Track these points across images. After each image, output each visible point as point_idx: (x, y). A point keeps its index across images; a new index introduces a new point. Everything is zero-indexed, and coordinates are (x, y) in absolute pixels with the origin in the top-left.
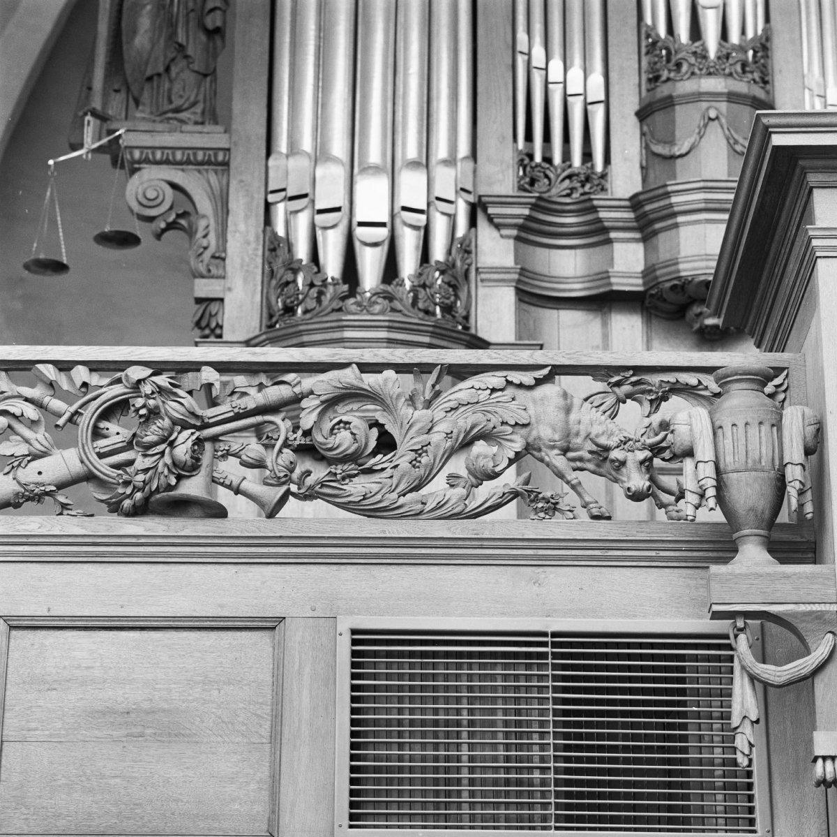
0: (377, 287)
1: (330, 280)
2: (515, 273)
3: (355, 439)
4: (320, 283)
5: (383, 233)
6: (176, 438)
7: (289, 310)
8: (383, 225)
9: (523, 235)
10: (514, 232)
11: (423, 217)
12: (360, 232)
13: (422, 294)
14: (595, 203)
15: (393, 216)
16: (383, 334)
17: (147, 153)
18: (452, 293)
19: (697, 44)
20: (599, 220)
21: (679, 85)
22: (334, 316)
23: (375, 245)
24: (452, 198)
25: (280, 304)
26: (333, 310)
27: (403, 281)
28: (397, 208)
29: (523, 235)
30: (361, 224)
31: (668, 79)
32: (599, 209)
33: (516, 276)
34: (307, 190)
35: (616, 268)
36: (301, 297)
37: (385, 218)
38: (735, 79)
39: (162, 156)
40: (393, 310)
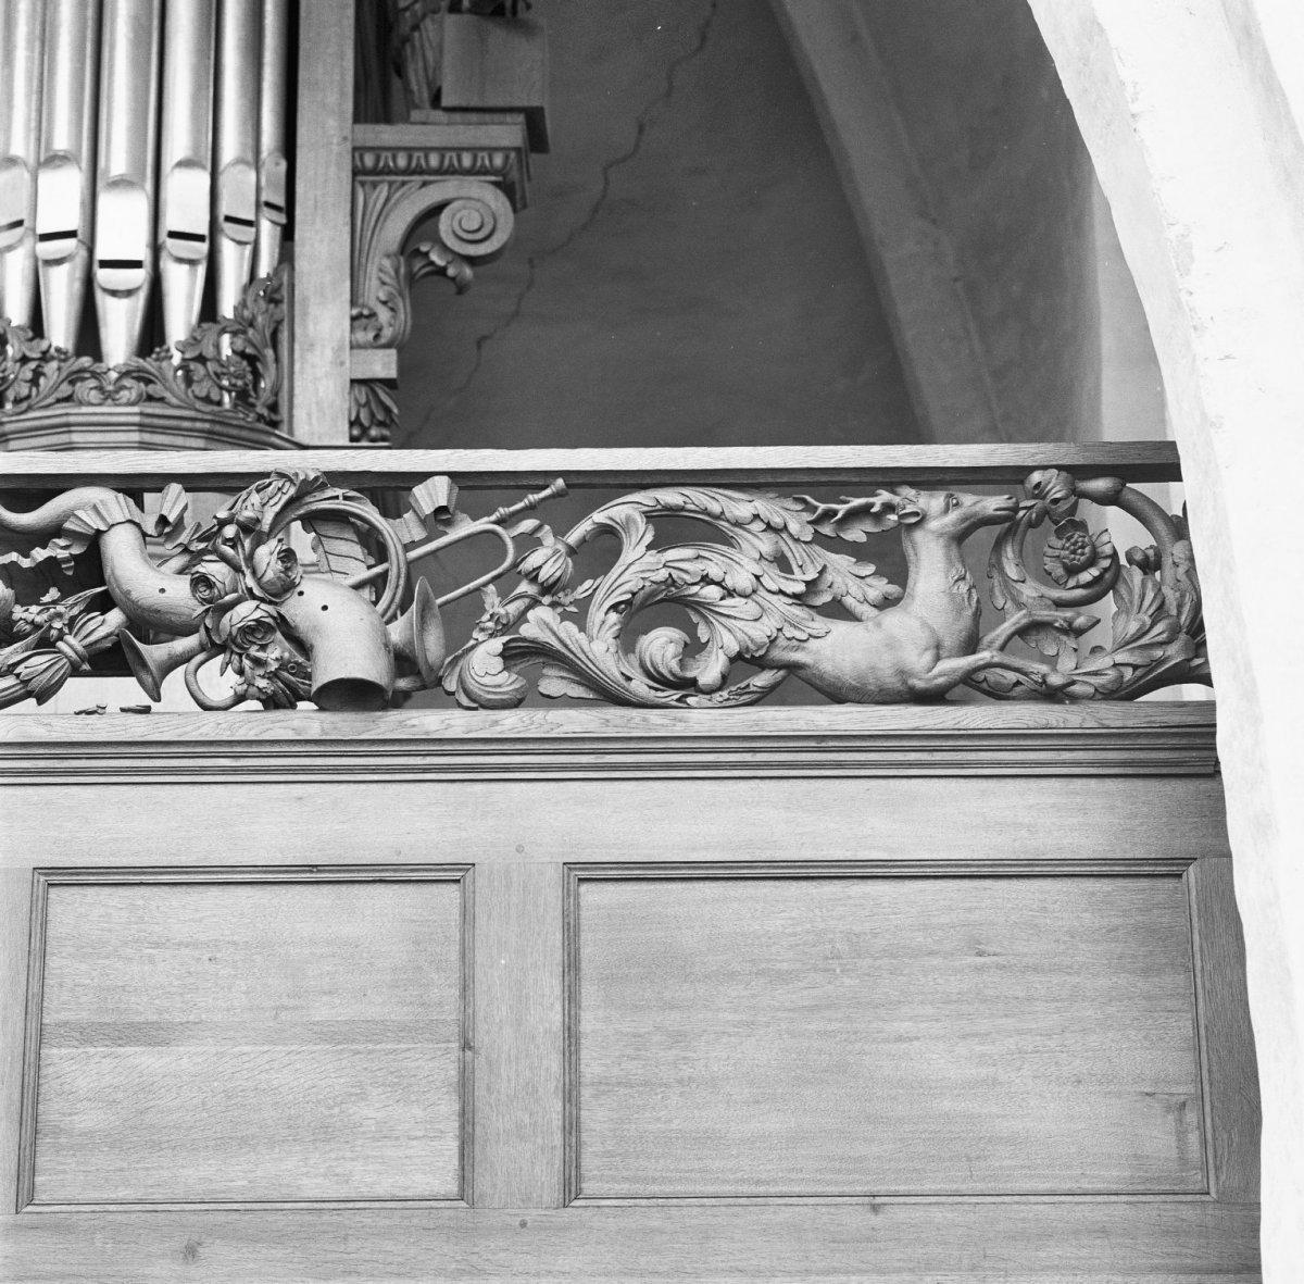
4: (39, 355)
5: (139, 277)
8: (137, 264)
12: (103, 276)
13: (198, 370)
15: (156, 249)
16: (135, 437)
17: (451, 158)
18: (248, 369)
22: (59, 410)
23: (129, 293)
26: (59, 401)
30: (105, 264)
34: (23, 215)
39: (442, 162)
40: (150, 398)
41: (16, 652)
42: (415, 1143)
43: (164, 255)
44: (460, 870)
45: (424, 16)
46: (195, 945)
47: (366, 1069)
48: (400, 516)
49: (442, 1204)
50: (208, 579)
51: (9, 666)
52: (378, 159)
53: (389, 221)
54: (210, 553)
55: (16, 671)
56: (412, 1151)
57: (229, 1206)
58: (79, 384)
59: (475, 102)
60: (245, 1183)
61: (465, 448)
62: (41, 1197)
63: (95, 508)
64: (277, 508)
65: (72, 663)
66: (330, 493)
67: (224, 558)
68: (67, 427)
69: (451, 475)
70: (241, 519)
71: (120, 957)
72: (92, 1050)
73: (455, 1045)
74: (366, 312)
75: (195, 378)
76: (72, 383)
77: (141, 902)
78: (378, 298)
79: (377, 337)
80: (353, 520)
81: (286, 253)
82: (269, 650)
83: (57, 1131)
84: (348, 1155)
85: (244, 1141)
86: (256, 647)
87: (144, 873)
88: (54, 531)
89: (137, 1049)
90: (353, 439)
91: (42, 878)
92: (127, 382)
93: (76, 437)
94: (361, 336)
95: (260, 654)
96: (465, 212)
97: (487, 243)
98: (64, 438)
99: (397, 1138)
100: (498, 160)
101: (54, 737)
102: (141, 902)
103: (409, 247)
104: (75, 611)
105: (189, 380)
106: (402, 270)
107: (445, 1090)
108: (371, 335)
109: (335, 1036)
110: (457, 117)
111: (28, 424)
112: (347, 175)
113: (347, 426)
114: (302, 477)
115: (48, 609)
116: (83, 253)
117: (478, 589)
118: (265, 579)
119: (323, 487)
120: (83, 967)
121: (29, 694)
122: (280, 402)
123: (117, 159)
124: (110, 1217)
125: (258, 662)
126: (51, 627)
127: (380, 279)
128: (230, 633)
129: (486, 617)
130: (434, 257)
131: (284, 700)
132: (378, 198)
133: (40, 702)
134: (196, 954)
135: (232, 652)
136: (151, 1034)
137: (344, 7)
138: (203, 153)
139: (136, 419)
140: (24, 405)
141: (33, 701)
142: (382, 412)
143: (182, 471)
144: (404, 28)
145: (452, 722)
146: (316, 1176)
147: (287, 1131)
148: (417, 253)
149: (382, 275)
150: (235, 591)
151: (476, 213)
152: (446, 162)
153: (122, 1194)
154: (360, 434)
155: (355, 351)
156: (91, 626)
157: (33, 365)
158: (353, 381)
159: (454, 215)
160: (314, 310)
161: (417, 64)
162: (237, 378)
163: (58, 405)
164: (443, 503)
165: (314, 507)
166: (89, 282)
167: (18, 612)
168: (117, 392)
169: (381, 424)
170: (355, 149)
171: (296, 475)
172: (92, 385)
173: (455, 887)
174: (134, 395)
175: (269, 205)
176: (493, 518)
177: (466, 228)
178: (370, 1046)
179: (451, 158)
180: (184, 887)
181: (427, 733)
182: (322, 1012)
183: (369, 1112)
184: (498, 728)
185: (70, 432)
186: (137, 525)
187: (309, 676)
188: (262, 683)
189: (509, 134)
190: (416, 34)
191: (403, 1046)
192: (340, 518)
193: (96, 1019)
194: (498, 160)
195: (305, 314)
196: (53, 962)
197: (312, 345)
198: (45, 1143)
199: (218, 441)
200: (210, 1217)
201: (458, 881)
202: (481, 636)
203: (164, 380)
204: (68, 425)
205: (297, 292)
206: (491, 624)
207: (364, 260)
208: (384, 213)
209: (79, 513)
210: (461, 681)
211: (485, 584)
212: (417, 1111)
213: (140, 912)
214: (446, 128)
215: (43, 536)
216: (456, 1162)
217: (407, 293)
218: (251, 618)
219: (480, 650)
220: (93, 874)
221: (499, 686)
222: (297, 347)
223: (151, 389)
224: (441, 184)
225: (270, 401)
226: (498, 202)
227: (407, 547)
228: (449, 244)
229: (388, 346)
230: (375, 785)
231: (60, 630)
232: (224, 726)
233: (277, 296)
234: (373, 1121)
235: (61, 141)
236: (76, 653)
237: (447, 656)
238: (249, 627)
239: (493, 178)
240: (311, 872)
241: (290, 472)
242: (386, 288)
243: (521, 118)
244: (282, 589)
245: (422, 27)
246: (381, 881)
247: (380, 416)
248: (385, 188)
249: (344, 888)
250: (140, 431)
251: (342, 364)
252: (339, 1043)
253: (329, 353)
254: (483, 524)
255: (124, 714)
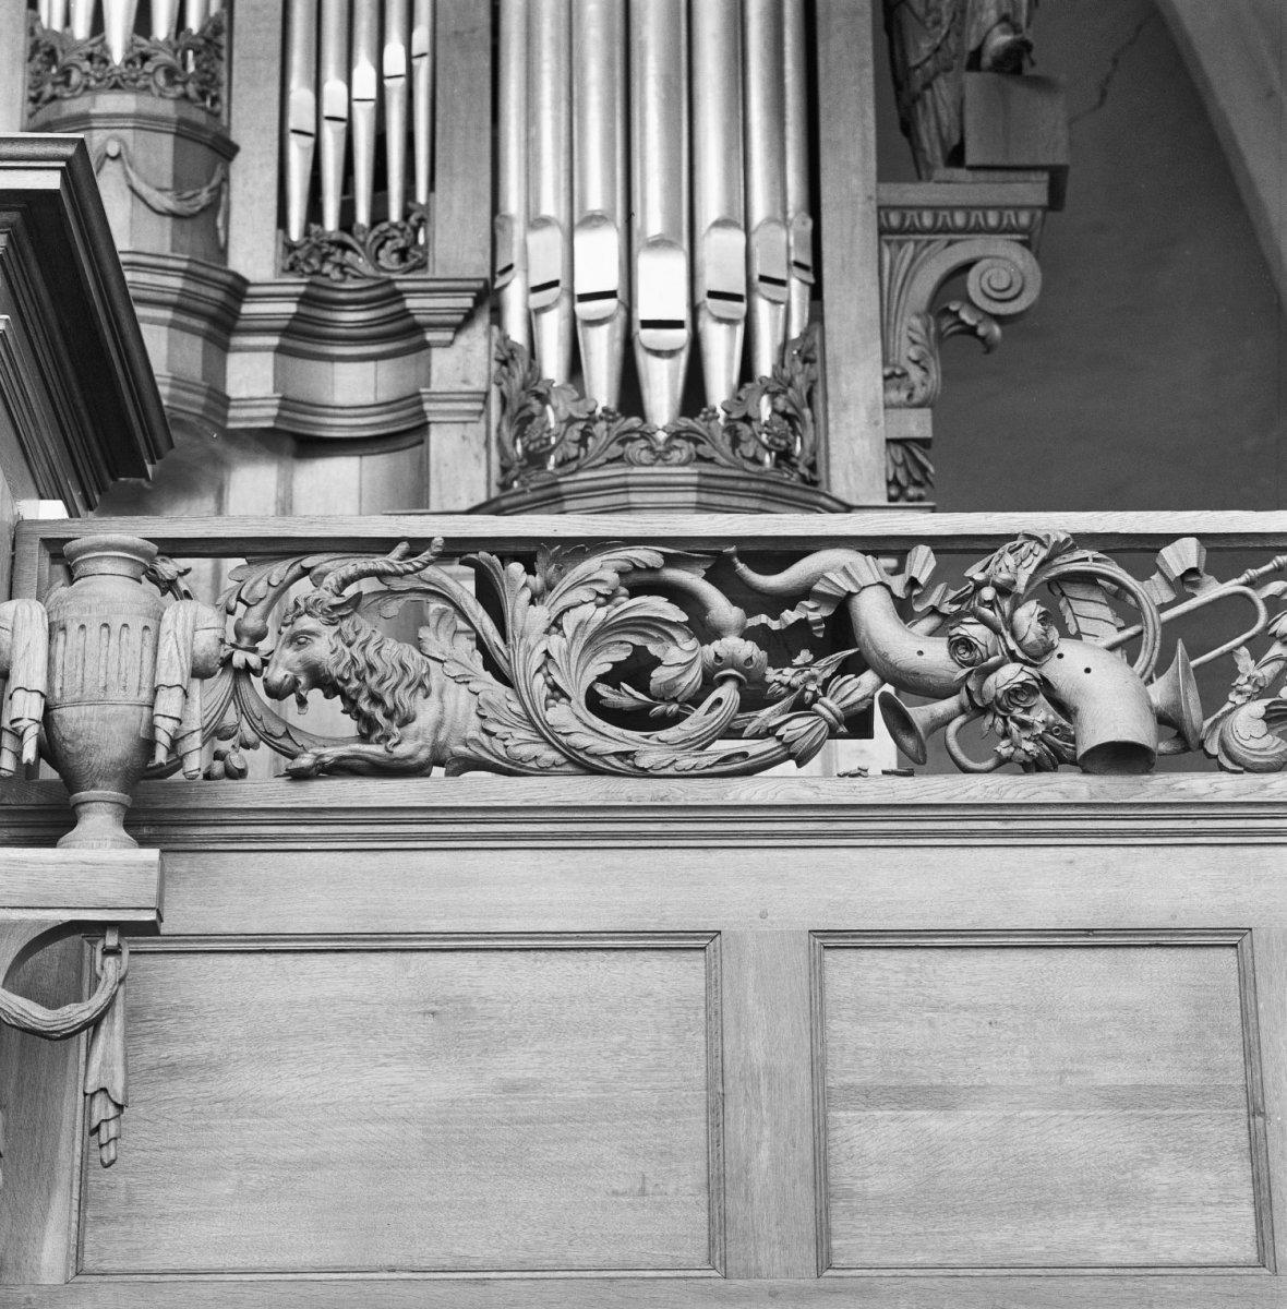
0: (674, 423)
1: (599, 411)
2: (272, 406)
3: (155, 691)
4: (585, 416)
5: (681, 337)
6: (950, 326)
7: (535, 459)
8: (678, 324)
9: (290, 343)
10: (274, 341)
11: (743, 306)
12: (646, 336)
14: (398, 286)
15: (694, 309)
16: (693, 497)
17: (977, 217)
18: (790, 429)
19: (95, 40)
20: (406, 313)
21: (66, 104)
23: (671, 354)
24: (781, 275)
25: (519, 448)
26: (610, 461)
27: (714, 411)
28: (701, 296)
29: (290, 343)
30: (647, 324)
31: (54, 98)
32: (405, 295)
33: (274, 412)
35: (434, 387)
36: (553, 441)
37: (682, 314)
38: (153, 95)
39: (1001, 220)
40: (700, 458)
41: (773, 714)
42: (1210, 1209)
43: (703, 315)
44: (706, 938)
45: (936, 74)
46: (974, 1008)
47: (1155, 1135)
48: (1149, 579)
49: (1245, 1271)
50: (968, 641)
51: (769, 729)
52: (903, 218)
53: (916, 282)
54: (968, 615)
55: (779, 733)
56: (1209, 1217)
57: (1029, 1272)
58: (629, 445)
59: (999, 161)
60: (1043, 1248)
61: (1212, 509)
62: (839, 1261)
63: (845, 570)
64: (1031, 570)
65: (830, 726)
66: (1078, 554)
67: (983, 621)
68: (626, 487)
69: (1199, 536)
70: (998, 581)
71: (900, 1021)
72: (878, 1114)
73: (1244, 1111)
74: (898, 372)
75: (743, 438)
76: (622, 443)
77: (916, 965)
78: (909, 358)
79: (910, 396)
80: (1100, 581)
81: (816, 314)
82: (1033, 712)
83: (850, 1194)
84: (1145, 1220)
85: (1038, 1206)
86: (1020, 710)
87: (919, 936)
88: (805, 592)
89: (924, 1113)
90: (891, 499)
91: (818, 941)
92: (677, 443)
93: (634, 498)
94: (894, 396)
95: (1025, 717)
96: (994, 271)
97: (1016, 302)
98: (621, 499)
99: (1192, 1205)
100: (1024, 219)
101: (823, 799)
102: (916, 965)
103: (938, 307)
104: (828, 673)
105: (736, 442)
106: (932, 330)
107: (1237, 1156)
108: (904, 395)
109: (1124, 1100)
110: (981, 175)
111: (577, 485)
112: (873, 233)
113: (884, 486)
114: (1053, 539)
115: (803, 671)
116: (622, 314)
117: (1231, 652)
118: (1027, 641)
119: (1072, 549)
120: (865, 1030)
121: (790, 756)
122: (818, 464)
123: (653, 221)
124: (911, 1282)
125: (1024, 725)
126: (805, 690)
127: (910, 338)
128: (996, 696)
129: (1241, 680)
130: (964, 316)
131: (1048, 762)
132: (903, 258)
133: (800, 763)
134: (977, 1018)
135: (995, 714)
136: (940, 1098)
137: (862, 65)
138: (736, 215)
139: (695, 479)
140: (573, 466)
141: (791, 763)
142: (914, 472)
143: (929, 533)
144: (917, 86)
145: (1221, 786)
146: (1114, 1242)
147: (1080, 1197)
148: (947, 311)
149: (911, 334)
150: (996, 654)
151: (1004, 272)
152: (1005, 222)
153: (919, 1258)
154: (899, 493)
155: (890, 411)
156: (848, 688)
157: (581, 426)
158: (889, 441)
159: (982, 275)
160: (845, 370)
161: (928, 122)
162: (780, 438)
163: (608, 466)
164: (1194, 564)
165: (1065, 569)
166: (629, 343)
167: (771, 674)
168: (667, 452)
169: (918, 484)
170: (880, 208)
171: (1048, 537)
172: (643, 446)
173: (701, 954)
174: (684, 455)
175: (798, 264)
176: (1242, 579)
177: (995, 286)
178: (1158, 1111)
179: (977, 217)
180: (960, 950)
181: (1196, 796)
182: (1110, 1075)
183: (1159, 1177)
184: (1268, 792)
185: (628, 492)
186: (888, 588)
187: (1073, 740)
188: (1029, 746)
189: (1034, 191)
190: (928, 93)
191: (1190, 1111)
192: (1088, 579)
193: (881, 1082)
194: (1024, 219)
195: (837, 374)
196: (834, 1026)
197: (845, 405)
198: (838, 1207)
199: (772, 501)
200: (1014, 1283)
201: (1235, 946)
202: (1239, 700)
203: (713, 441)
204: (626, 485)
205: (828, 352)
206: (1248, 687)
207: (893, 320)
208: (910, 274)
209: (830, 575)
210: (1223, 745)
211: (1237, 647)
212: (1209, 1177)
213: (917, 975)
214: (972, 187)
215: (790, 599)
216: (1252, 1227)
217: (937, 352)
218: (1016, 680)
219: (1243, 713)
220: (869, 937)
221: (1265, 749)
222: (830, 407)
223: (701, 449)
224: (968, 243)
225: (809, 462)
226: (1022, 260)
227: (1163, 608)
228: (978, 303)
229: (920, 406)
230: (1145, 849)
231: (815, 692)
232: (992, 789)
233: (811, 356)
234: (1165, 1187)
235: (595, 201)
236: (834, 714)
237: (1205, 718)
238: (1014, 690)
239: (1019, 237)
240: (1087, 936)
241: (1041, 535)
242: (917, 347)
243: (1045, 177)
244: (1037, 655)
245: (934, 84)
246: (1158, 946)
247: (917, 476)
248: (911, 246)
249: (1120, 952)
250: (697, 491)
251: (876, 423)
252: (1125, 1109)
253: (863, 413)
254: (1232, 586)
255: (886, 777)
